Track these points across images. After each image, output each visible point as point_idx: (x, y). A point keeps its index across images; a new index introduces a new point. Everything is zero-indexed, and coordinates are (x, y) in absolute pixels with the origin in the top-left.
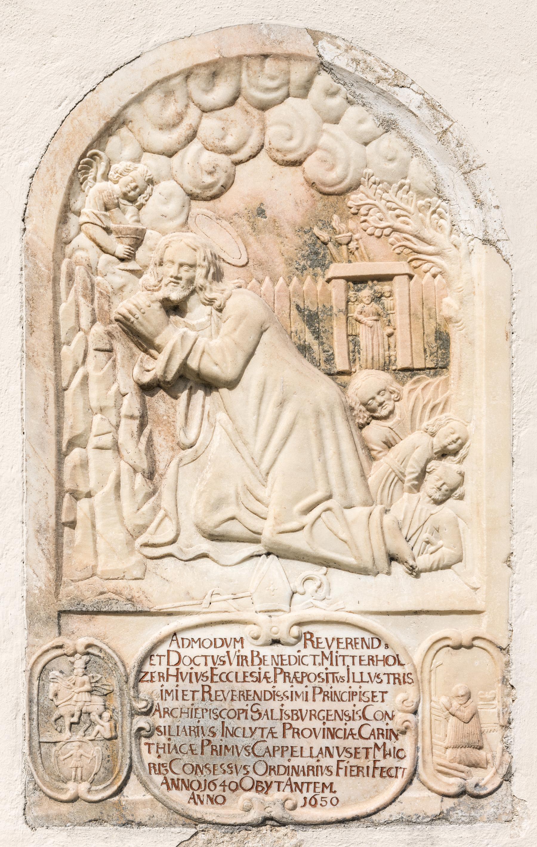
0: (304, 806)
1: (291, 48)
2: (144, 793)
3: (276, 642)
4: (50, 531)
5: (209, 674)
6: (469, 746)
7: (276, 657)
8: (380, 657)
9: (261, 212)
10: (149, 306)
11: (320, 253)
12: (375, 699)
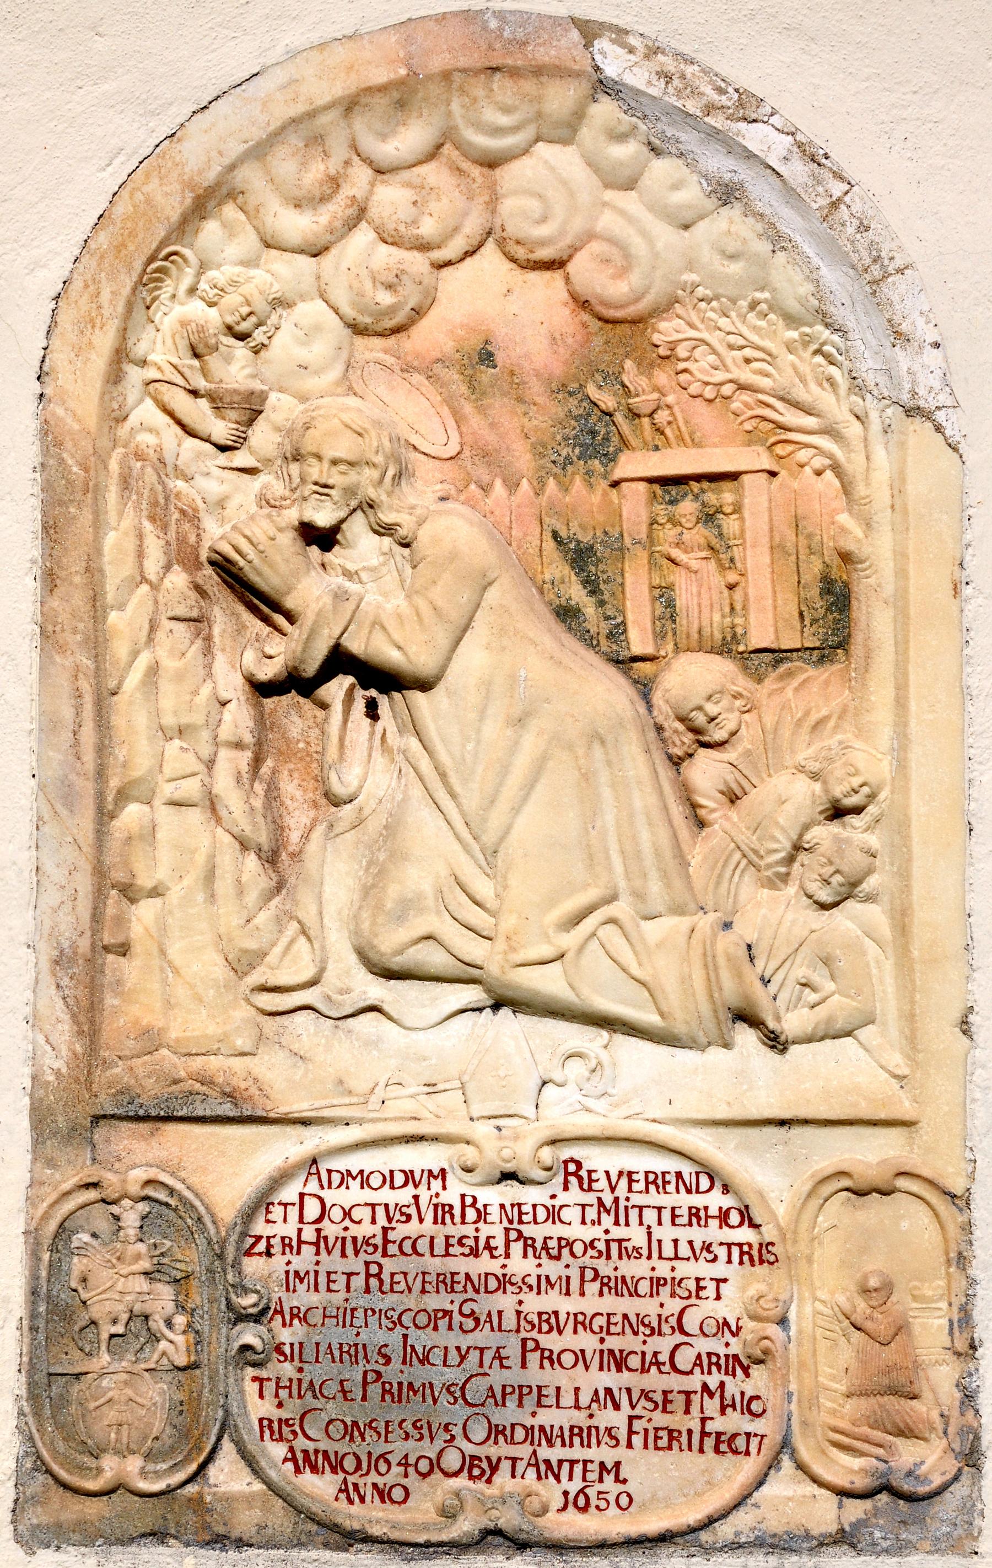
0: (565, 1508)
1: (543, 54)
2: (249, 1480)
3: (508, 1176)
4: (80, 962)
5: (379, 1241)
6: (894, 1391)
7: (508, 1208)
8: (713, 1211)
9: (487, 357)
10: (273, 539)
11: (597, 433)
12: (702, 1294)
